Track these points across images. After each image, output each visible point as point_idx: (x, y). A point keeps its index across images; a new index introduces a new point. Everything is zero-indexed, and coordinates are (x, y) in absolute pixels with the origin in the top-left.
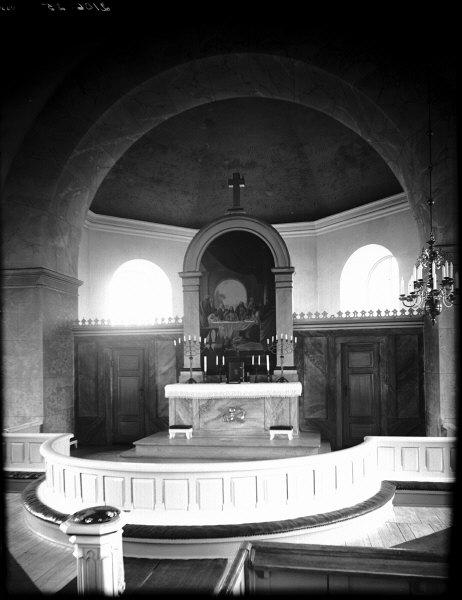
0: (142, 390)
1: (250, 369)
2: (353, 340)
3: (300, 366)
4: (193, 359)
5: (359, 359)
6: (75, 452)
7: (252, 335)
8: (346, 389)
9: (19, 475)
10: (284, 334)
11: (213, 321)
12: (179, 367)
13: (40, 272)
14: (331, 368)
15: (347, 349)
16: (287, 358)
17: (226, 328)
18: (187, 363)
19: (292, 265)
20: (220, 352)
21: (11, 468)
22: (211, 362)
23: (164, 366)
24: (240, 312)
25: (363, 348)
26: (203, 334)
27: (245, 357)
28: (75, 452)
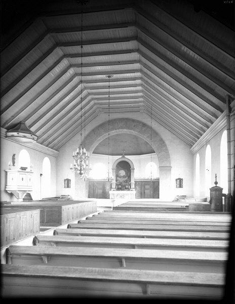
0: (103, 192)
1: (126, 188)
2: (146, 183)
3: (135, 188)
4: (114, 186)
5: (147, 187)
6: (222, 189)
7: (126, 181)
8: (144, 193)
9: (219, 210)
10: (133, 181)
11: (118, 178)
12: (111, 188)
13: (167, 151)
14: (141, 188)
15: (121, 188)
16: (133, 186)
17: (121, 180)
18: (113, 187)
19: (172, 165)
20: (120, 185)
21: (4, 273)
22: (118, 187)
23: (108, 187)
24: (124, 177)
25: (149, 185)
26: (116, 181)
27: (125, 186)
28: (222, 189)
